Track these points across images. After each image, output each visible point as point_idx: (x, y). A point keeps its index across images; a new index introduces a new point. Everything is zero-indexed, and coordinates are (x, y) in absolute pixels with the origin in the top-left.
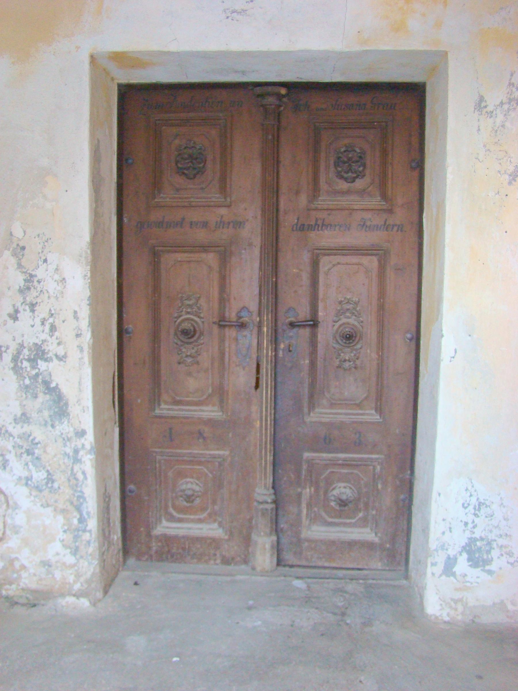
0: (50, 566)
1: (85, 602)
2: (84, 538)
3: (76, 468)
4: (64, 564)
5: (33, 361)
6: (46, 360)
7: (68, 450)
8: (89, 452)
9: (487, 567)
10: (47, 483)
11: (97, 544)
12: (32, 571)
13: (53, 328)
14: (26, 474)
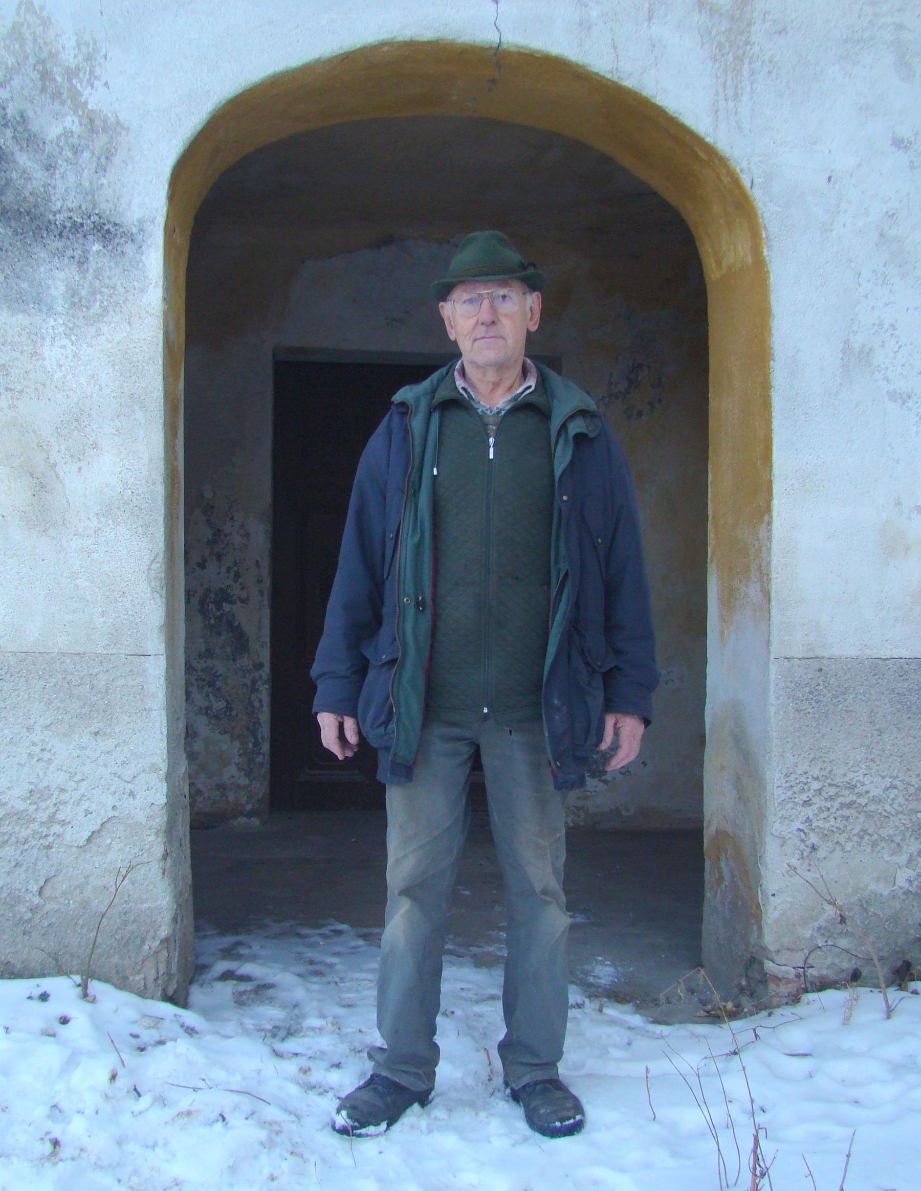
0: (224, 789)
1: (256, 821)
2: (257, 760)
3: (253, 697)
4: (238, 786)
5: (219, 606)
6: (231, 603)
7: (247, 681)
8: (266, 682)
9: (603, 778)
10: (226, 712)
11: (268, 766)
12: (206, 795)
13: (237, 576)
14: (207, 704)
